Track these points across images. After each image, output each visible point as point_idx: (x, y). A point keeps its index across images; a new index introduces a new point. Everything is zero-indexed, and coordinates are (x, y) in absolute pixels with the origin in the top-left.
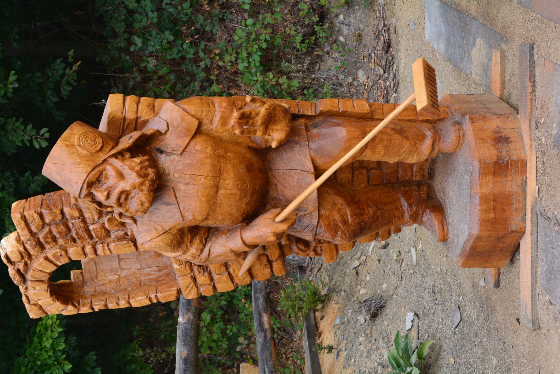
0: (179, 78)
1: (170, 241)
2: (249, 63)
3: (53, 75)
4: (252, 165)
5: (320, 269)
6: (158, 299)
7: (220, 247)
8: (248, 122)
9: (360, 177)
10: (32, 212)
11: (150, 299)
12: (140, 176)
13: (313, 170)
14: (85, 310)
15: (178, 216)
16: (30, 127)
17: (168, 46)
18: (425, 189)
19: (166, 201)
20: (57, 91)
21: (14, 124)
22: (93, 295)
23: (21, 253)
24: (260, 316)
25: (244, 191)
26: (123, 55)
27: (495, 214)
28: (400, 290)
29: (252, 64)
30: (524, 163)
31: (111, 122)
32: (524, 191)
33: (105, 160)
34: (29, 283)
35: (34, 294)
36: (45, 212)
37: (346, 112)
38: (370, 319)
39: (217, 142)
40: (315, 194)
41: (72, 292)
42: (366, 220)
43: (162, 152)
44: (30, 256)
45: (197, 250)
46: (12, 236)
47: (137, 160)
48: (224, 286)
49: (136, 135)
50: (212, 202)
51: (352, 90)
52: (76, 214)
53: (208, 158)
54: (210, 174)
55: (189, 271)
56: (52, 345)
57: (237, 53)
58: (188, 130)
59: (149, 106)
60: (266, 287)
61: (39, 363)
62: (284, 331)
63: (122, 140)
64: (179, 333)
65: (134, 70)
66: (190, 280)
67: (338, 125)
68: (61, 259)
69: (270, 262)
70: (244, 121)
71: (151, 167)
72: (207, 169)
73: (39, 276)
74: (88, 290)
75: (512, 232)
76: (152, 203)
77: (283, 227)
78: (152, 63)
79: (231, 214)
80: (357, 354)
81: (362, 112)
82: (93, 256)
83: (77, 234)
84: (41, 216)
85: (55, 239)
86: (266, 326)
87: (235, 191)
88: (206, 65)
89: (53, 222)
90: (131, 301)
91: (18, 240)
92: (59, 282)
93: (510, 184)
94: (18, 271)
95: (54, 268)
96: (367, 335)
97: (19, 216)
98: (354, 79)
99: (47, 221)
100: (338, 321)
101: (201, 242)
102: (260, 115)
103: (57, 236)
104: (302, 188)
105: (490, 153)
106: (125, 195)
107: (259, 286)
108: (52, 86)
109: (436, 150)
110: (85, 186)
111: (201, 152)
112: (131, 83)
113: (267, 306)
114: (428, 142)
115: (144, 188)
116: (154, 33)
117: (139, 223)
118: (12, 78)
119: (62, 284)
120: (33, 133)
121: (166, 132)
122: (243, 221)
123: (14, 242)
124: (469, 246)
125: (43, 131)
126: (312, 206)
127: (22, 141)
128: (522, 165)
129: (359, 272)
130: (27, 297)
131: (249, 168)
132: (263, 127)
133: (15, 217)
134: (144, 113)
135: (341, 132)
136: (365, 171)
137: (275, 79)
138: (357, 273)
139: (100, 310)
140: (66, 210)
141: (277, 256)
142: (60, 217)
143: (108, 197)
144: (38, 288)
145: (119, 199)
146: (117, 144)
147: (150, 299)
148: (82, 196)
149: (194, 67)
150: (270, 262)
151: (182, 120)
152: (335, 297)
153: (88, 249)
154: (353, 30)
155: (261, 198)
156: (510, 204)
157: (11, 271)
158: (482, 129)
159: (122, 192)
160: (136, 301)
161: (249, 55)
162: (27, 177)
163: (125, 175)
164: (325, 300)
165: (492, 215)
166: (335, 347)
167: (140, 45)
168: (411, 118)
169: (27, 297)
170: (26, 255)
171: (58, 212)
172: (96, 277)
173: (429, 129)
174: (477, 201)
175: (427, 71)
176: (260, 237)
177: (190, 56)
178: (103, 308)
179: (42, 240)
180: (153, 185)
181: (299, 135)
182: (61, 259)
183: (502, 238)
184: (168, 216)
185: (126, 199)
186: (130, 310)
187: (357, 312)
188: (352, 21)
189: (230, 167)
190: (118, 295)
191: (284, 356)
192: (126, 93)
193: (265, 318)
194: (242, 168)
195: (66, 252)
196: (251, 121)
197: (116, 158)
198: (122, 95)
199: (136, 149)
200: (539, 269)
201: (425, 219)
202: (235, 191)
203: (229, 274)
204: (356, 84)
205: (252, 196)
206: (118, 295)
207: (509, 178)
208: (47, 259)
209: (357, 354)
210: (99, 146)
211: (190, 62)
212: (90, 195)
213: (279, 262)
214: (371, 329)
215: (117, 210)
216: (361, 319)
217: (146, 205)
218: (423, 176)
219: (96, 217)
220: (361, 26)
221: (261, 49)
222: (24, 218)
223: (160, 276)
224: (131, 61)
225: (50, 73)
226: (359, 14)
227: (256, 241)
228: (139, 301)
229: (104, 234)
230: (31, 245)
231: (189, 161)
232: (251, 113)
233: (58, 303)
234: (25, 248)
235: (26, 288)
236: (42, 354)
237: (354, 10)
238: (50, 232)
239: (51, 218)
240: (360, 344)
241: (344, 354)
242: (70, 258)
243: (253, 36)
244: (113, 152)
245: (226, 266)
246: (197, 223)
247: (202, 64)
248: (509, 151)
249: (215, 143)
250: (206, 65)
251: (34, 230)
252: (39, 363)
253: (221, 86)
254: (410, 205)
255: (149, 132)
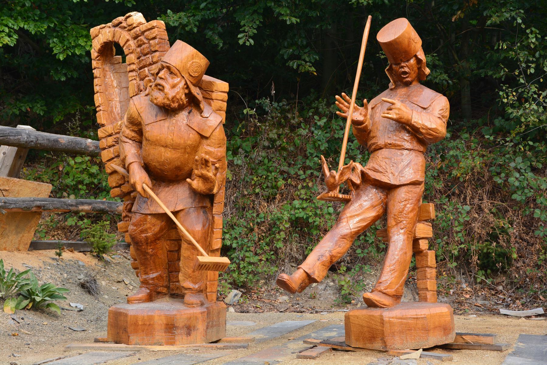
0: (290, 154)
1: (133, 116)
2: (298, 209)
3: (305, 53)
4: (180, 171)
5: (126, 258)
6: (99, 111)
7: (130, 151)
8: (203, 164)
9: (173, 245)
10: (157, 33)
11: (99, 106)
12: (173, 98)
13: (176, 210)
14: (94, 64)
15: (149, 122)
16: (255, 31)
17: (317, 145)
18: (164, 291)
19: (159, 114)
20: (293, 57)
21: (258, 20)
22: (104, 69)
23: (132, 25)
24: (89, 204)
25: (163, 164)
26: (312, 110)
27: (141, 325)
28: (102, 305)
29: (297, 211)
30: (172, 344)
31: (211, 83)
32: (155, 344)
33: (183, 77)
34: (113, 29)
35: (106, 32)
36: (157, 41)
37: (213, 233)
38: (81, 283)
39: (195, 148)
40: (161, 211)
41: (107, 56)
42: (143, 247)
43: (189, 113)
44: (130, 30)
45: (128, 134)
46: (143, 20)
47: (183, 97)
48: (105, 155)
49: (200, 97)
50: (156, 143)
51: (273, 292)
52: (155, 60)
53: (184, 141)
54: (174, 142)
55: (116, 131)
56: (80, 45)
57: (306, 200)
58: (203, 130)
59: (220, 107)
60: (112, 212)
61: (66, 35)
62: (77, 234)
63: (198, 89)
64: (79, 139)
65: (301, 119)
66: (110, 132)
67: (204, 226)
68: (127, 50)
69: (119, 186)
70: (204, 162)
71: (179, 105)
72: (177, 141)
73: (117, 35)
74: (107, 67)
75: (129, 337)
76: (156, 105)
77: (139, 188)
78: (303, 132)
79: (149, 155)
80: (53, 271)
81: (213, 243)
82: (128, 70)
83: (142, 60)
84: (154, 38)
85: (139, 46)
86: (81, 208)
87: (163, 158)
88: (300, 176)
89: (150, 46)
90: (99, 94)
91: (140, 24)
92: (114, 48)
93: (160, 335)
94: (121, 23)
95: (122, 45)
96: (68, 280)
97: (155, 24)
98: (281, 293)
99: (151, 42)
100: (80, 263)
101: (133, 137)
102: (207, 173)
103: (142, 48)
104: (165, 203)
105: (180, 323)
106: (160, 88)
107: (113, 206)
108: (296, 53)
109: (186, 292)
110: (168, 65)
111: (189, 138)
112: (289, 116)
113: (97, 211)
114: (191, 285)
115: (166, 100)
116: (328, 135)
117: (146, 97)
118: (294, 20)
119: (112, 50)
120: (251, 34)
121: (202, 116)
122: (145, 163)
123: (139, 21)
124: (122, 311)
125: (252, 41)
126: (153, 210)
127: (244, 25)
128: (171, 343)
129: (120, 284)
130: (104, 27)
131: (178, 168)
132: (200, 175)
133: (154, 23)
134: (216, 104)
135: (198, 228)
136: (177, 249)
137: (284, 229)
138: (119, 282)
139: (93, 73)
140: (157, 54)
141: (124, 191)
142: (153, 50)
143: (161, 78)
144: (109, 34)
145: (159, 85)
146: (194, 85)
147: (99, 106)
148: (162, 63)
149: (299, 166)
150: (119, 186)
151: (210, 127)
152: (100, 264)
153: (133, 67)
154: (320, 293)
155: (161, 176)
156: (147, 335)
157: (121, 18)
158: (197, 318)
159: (163, 87)
160: (98, 97)
161: (303, 209)
162: (217, 29)
163: (174, 88)
164: (99, 258)
165: (140, 323)
166: (61, 257)
167: (319, 123)
168: (208, 277)
169: (104, 27)
170: (131, 28)
171: (156, 49)
172: (117, 72)
173: (200, 287)
174: (150, 314)
175: (222, 265)
176: (134, 173)
177: (308, 163)
178: (94, 76)
179: (139, 38)
180: (167, 106)
181: (199, 202)
182: (127, 50)
183: (126, 331)
184: (148, 116)
185: (160, 89)
186: (93, 93)
187: (86, 275)
188: (328, 292)
189: (179, 155)
190: (103, 85)
191: (56, 233)
192: (229, 93)
193: (86, 207)
194: (178, 163)
195: (132, 53)
196: (203, 166)
197: (185, 84)
198: (228, 91)
199: (190, 96)
200: (103, 352)
201: (143, 289)
202: (163, 158)
203: (113, 158)
204: (277, 294)
205: (160, 169)
206: (103, 85)
207: (164, 334)
208: (128, 40)
209: (53, 271)
210: (192, 74)
211: (304, 163)
212: (163, 68)
213: (120, 192)
214: (73, 283)
215: (153, 84)
216: (82, 276)
217: (155, 101)
218: (173, 290)
219: (152, 72)
220: (322, 299)
221: (308, 218)
222: (153, 28)
223: (114, 114)
224: (308, 116)
225: (306, 50)
226: (332, 297)
227: (131, 172)
228: (98, 99)
229: (142, 77)
230: (137, 31)
231: (183, 129)
232: (208, 167)
233: (99, 46)
234: (135, 27)
235: (110, 27)
236: (73, 37)
237: (336, 293)
238: (144, 43)
239: (153, 44)
240: (61, 274)
241: (55, 263)
242: (127, 55)
243: (318, 212)
244: (188, 82)
245: (118, 156)
246: (144, 134)
247: (301, 172)
248: (181, 334)
249: (194, 147)
250: (300, 176)
251: (146, 34)
252: (66, 35)
253: (283, 187)
254: (153, 279)
255: (202, 106)
